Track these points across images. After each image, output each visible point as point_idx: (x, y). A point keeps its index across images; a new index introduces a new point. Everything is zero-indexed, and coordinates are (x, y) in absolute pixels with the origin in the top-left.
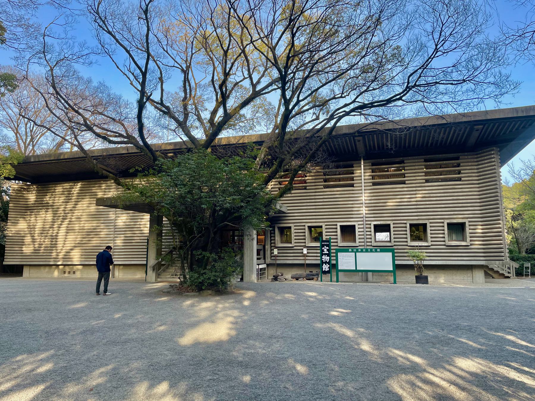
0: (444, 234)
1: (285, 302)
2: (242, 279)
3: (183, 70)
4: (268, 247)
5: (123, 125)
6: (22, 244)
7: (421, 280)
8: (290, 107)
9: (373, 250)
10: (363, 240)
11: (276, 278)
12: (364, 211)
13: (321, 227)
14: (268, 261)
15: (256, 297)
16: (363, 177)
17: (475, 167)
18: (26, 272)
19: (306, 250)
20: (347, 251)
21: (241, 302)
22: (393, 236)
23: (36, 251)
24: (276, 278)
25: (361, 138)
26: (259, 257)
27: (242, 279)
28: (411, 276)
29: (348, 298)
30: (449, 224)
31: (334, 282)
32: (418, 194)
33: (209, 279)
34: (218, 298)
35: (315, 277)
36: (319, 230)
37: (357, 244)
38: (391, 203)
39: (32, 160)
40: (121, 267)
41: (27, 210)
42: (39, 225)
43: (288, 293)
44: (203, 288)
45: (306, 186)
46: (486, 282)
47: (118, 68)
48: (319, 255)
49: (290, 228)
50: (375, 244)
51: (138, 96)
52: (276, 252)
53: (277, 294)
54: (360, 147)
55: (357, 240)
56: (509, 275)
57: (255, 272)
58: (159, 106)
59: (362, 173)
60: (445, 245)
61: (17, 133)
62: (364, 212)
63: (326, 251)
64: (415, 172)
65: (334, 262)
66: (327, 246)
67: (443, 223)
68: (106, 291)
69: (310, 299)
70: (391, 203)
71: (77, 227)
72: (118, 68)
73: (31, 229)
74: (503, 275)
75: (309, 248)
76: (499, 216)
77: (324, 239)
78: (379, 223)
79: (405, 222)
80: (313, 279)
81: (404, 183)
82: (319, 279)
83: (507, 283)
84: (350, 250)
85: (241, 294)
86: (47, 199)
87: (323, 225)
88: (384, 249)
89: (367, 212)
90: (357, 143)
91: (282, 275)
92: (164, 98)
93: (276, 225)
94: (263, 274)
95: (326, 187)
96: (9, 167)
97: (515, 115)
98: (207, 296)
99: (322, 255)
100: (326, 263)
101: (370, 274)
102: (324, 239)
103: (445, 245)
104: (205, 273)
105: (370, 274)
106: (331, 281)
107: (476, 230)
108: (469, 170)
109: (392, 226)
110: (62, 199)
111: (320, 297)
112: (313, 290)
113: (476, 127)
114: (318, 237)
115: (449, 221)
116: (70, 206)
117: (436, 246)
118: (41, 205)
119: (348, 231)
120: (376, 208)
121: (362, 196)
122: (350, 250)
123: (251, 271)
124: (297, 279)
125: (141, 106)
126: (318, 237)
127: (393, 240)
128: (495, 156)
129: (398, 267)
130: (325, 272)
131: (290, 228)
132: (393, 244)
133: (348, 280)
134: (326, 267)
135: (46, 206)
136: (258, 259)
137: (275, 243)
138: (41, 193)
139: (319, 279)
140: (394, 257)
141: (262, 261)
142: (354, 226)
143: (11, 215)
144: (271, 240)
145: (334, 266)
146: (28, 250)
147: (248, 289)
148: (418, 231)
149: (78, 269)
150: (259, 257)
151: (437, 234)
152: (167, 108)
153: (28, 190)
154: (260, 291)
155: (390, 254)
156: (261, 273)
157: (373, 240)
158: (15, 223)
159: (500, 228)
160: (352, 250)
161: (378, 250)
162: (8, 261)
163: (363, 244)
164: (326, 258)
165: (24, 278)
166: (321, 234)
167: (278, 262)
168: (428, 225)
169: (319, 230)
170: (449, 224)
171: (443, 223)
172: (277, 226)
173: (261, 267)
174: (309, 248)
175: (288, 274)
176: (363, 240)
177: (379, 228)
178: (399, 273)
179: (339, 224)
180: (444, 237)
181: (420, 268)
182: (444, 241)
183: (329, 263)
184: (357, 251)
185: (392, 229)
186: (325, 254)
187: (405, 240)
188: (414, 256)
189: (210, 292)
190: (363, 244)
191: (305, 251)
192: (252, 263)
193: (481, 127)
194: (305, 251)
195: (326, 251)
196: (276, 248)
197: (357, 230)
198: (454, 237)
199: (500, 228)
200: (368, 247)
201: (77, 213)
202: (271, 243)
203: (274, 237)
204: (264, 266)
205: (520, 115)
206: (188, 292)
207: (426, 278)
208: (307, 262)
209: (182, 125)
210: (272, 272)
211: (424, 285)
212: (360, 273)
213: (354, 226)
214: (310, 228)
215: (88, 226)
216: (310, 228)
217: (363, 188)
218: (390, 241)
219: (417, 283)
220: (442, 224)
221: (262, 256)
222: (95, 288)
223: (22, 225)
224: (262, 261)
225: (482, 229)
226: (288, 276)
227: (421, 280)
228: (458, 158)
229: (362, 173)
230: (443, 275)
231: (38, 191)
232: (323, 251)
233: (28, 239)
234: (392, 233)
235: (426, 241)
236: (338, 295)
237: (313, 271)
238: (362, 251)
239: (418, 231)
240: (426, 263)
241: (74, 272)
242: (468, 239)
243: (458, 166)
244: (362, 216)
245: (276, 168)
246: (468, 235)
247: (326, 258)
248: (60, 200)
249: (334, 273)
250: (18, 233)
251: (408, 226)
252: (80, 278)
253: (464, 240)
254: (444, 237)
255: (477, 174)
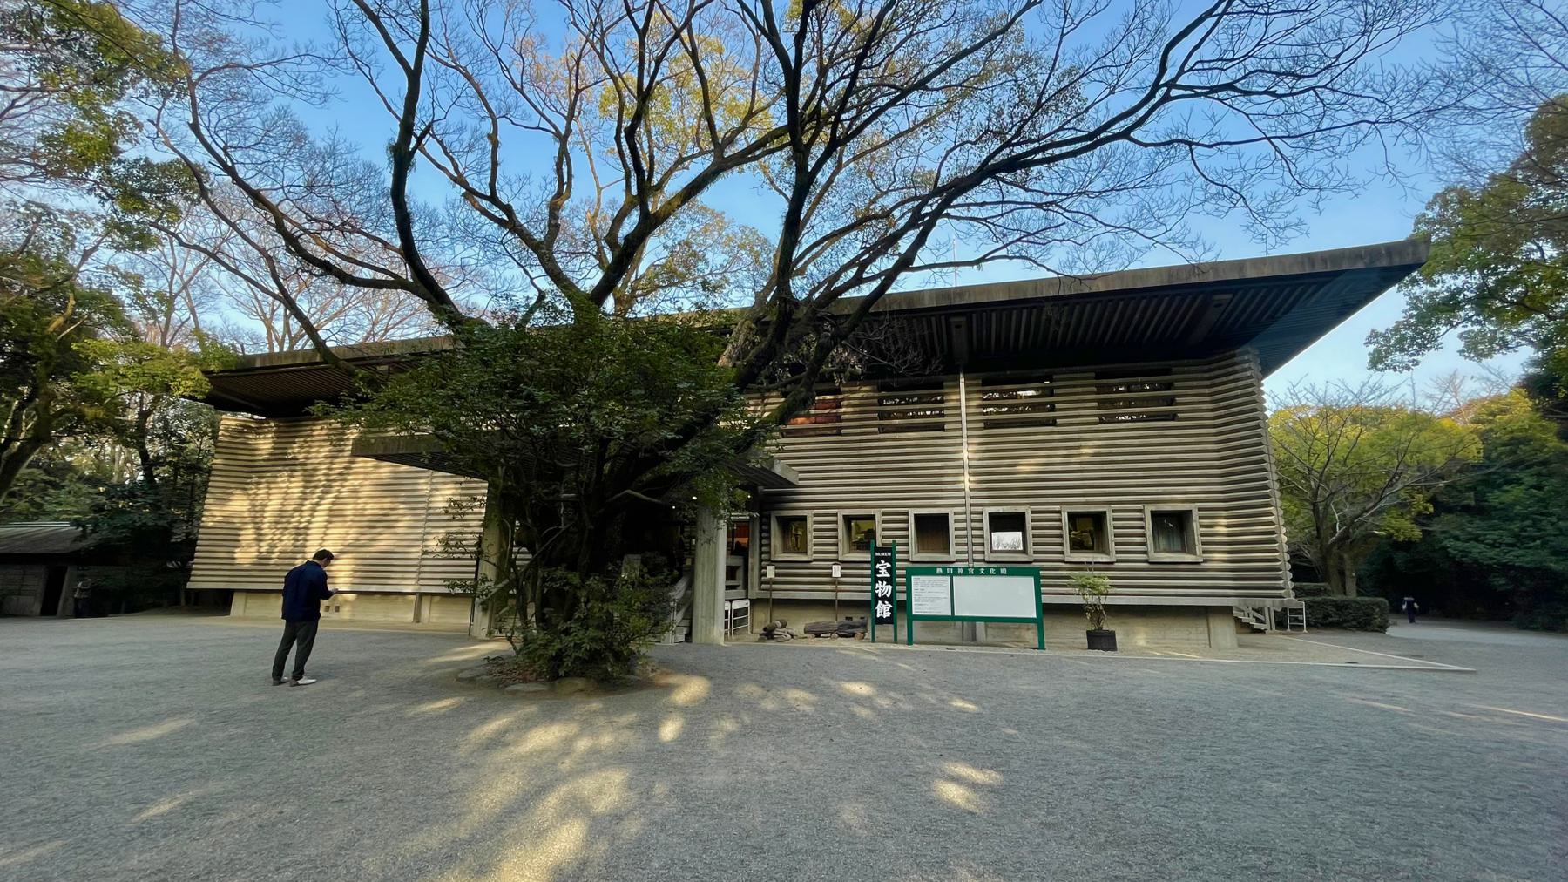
0: (1143, 535)
1: (783, 726)
2: (688, 637)
3: (557, 134)
4: (753, 561)
5: (409, 252)
6: (234, 542)
7: (1101, 640)
8: (812, 163)
9: (971, 571)
10: (965, 548)
11: (769, 634)
12: (967, 481)
13: (872, 518)
14: (755, 592)
15: (707, 701)
16: (963, 410)
17: (1207, 391)
18: (238, 605)
19: (839, 570)
20: (932, 572)
21: (653, 725)
22: (1031, 540)
23: (262, 560)
24: (769, 634)
25: (963, 319)
26: (731, 583)
27: (688, 637)
28: (1077, 632)
29: (959, 704)
30: (1154, 515)
31: (902, 643)
32: (1089, 449)
33: (577, 646)
34: (596, 705)
35: (858, 632)
36: (865, 525)
37: (953, 556)
38: (1025, 467)
39: (258, 365)
40: (437, 599)
41: (250, 472)
42: (274, 504)
43: (797, 686)
44: (562, 673)
45: (840, 428)
46: (1240, 646)
47: (389, 108)
48: (869, 580)
49: (804, 519)
50: (992, 558)
51: (394, 131)
52: (771, 572)
53: (767, 687)
54: (960, 339)
55: (953, 549)
56: (1262, 627)
57: (721, 619)
58: (485, 204)
59: (962, 399)
60: (1146, 561)
61: (270, 328)
62: (967, 485)
63: (884, 574)
64: (1078, 404)
65: (902, 597)
66: (887, 559)
67: (1140, 511)
68: (299, 673)
69: (857, 709)
70: (1025, 467)
71: (349, 509)
72: (389, 108)
73: (257, 511)
74: (1248, 625)
75: (845, 565)
76: (1268, 496)
77: (879, 545)
78: (1000, 510)
79: (1057, 508)
80: (853, 635)
81: (1054, 424)
82: (868, 635)
83: (1283, 649)
84: (939, 571)
85: (669, 689)
86: (295, 450)
87: (877, 513)
88: (1016, 570)
89: (974, 486)
90: (954, 331)
91: (784, 626)
92: (499, 182)
93: (769, 507)
94: (742, 621)
95: (883, 429)
96: (198, 374)
97: (1308, 270)
98: (572, 694)
99: (876, 580)
100: (884, 599)
101: (980, 625)
102: (879, 545)
103: (1146, 561)
104: (567, 632)
105: (980, 625)
106: (896, 642)
107: (1214, 528)
108: (1194, 399)
109: (1029, 517)
110: (325, 450)
111: (884, 703)
112: (862, 674)
113: (1217, 297)
114: (865, 541)
115: (1154, 507)
116: (339, 465)
117: (1127, 565)
118: (282, 461)
119: (933, 529)
120: (990, 477)
121: (963, 452)
122: (939, 571)
123: (711, 618)
124: (818, 636)
125: (402, 159)
126: (865, 541)
127: (1031, 548)
128: (1252, 365)
129: (1046, 610)
130: (881, 621)
131: (804, 519)
132: (1031, 556)
133: (931, 638)
134: (883, 610)
135: (291, 465)
136: (728, 587)
137: (769, 553)
138: (285, 437)
139: (868, 635)
140: (1038, 586)
141: (740, 592)
142: (946, 516)
143: (215, 482)
144: (761, 546)
145: (902, 607)
146: (245, 556)
147: (692, 670)
148: (1088, 529)
149: (346, 601)
150: (731, 583)
151: (1129, 533)
152: (507, 209)
153: (257, 431)
154: (722, 674)
155: (1032, 579)
156: (736, 621)
157: (987, 549)
158: (223, 501)
159: (1271, 523)
160: (944, 570)
161: (1003, 571)
162: (198, 582)
163: (965, 556)
164: (884, 589)
165: (239, 619)
166: (871, 534)
167: (776, 595)
168: (1110, 516)
169: (865, 525)
170: (1154, 515)
171: (1140, 511)
172: (774, 515)
173: (737, 605)
174: (845, 565)
175: (798, 624)
176: (965, 548)
177: (1002, 522)
178: (1047, 623)
179: (912, 512)
180: (1144, 544)
181: (1099, 612)
182: (1145, 552)
183: (891, 600)
184: (956, 572)
185: (1029, 524)
186: (882, 579)
187: (1059, 548)
188: (1084, 586)
189: (580, 683)
190: (965, 556)
191: (837, 572)
192: (716, 598)
193: (1229, 296)
194: (837, 572)
195: (884, 574)
196: (772, 563)
197: (952, 525)
198: (1163, 543)
199: (1271, 523)
200: (976, 565)
201: (352, 481)
202: (761, 553)
203: (769, 538)
204: (745, 604)
205: (1319, 269)
206: (525, 681)
207: (1112, 635)
208: (842, 596)
209: (543, 251)
210: (762, 618)
211: (1109, 654)
212: (959, 624)
213: (946, 516)
214: (848, 519)
215: (372, 507)
216: (848, 519)
217: (965, 432)
218: (1024, 552)
219: (1091, 647)
220: (1138, 515)
221: (739, 582)
222: (269, 668)
223: (239, 504)
224: (740, 592)
225: (1227, 526)
226: (798, 627)
227: (1101, 640)
228: (1167, 372)
229: (962, 399)
230: (1142, 629)
231: (279, 435)
232: (877, 571)
233: (248, 535)
234: (1030, 533)
235: (1105, 551)
236: (927, 691)
237: (854, 617)
238: (966, 573)
239: (1088, 529)
240: (1111, 601)
241: (337, 609)
242: (1199, 548)
243: (1169, 386)
244: (961, 494)
245: (769, 344)
246: (1198, 539)
247: (884, 589)
248: (320, 452)
249: (902, 623)
250: (227, 520)
251: (1065, 517)
252: (351, 621)
253: (1187, 547)
254: (1144, 544)
255: (1210, 406)
